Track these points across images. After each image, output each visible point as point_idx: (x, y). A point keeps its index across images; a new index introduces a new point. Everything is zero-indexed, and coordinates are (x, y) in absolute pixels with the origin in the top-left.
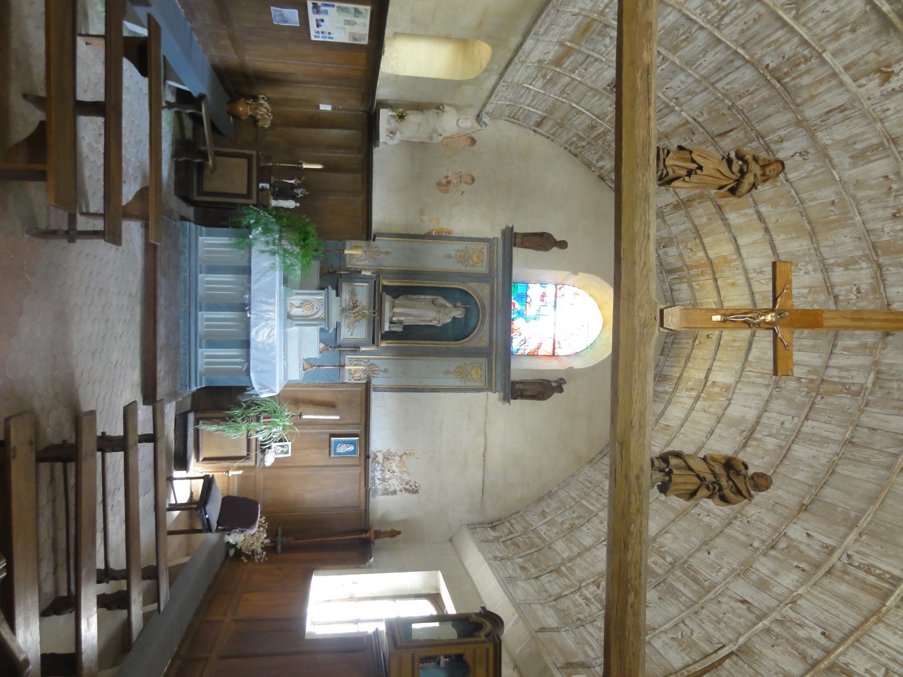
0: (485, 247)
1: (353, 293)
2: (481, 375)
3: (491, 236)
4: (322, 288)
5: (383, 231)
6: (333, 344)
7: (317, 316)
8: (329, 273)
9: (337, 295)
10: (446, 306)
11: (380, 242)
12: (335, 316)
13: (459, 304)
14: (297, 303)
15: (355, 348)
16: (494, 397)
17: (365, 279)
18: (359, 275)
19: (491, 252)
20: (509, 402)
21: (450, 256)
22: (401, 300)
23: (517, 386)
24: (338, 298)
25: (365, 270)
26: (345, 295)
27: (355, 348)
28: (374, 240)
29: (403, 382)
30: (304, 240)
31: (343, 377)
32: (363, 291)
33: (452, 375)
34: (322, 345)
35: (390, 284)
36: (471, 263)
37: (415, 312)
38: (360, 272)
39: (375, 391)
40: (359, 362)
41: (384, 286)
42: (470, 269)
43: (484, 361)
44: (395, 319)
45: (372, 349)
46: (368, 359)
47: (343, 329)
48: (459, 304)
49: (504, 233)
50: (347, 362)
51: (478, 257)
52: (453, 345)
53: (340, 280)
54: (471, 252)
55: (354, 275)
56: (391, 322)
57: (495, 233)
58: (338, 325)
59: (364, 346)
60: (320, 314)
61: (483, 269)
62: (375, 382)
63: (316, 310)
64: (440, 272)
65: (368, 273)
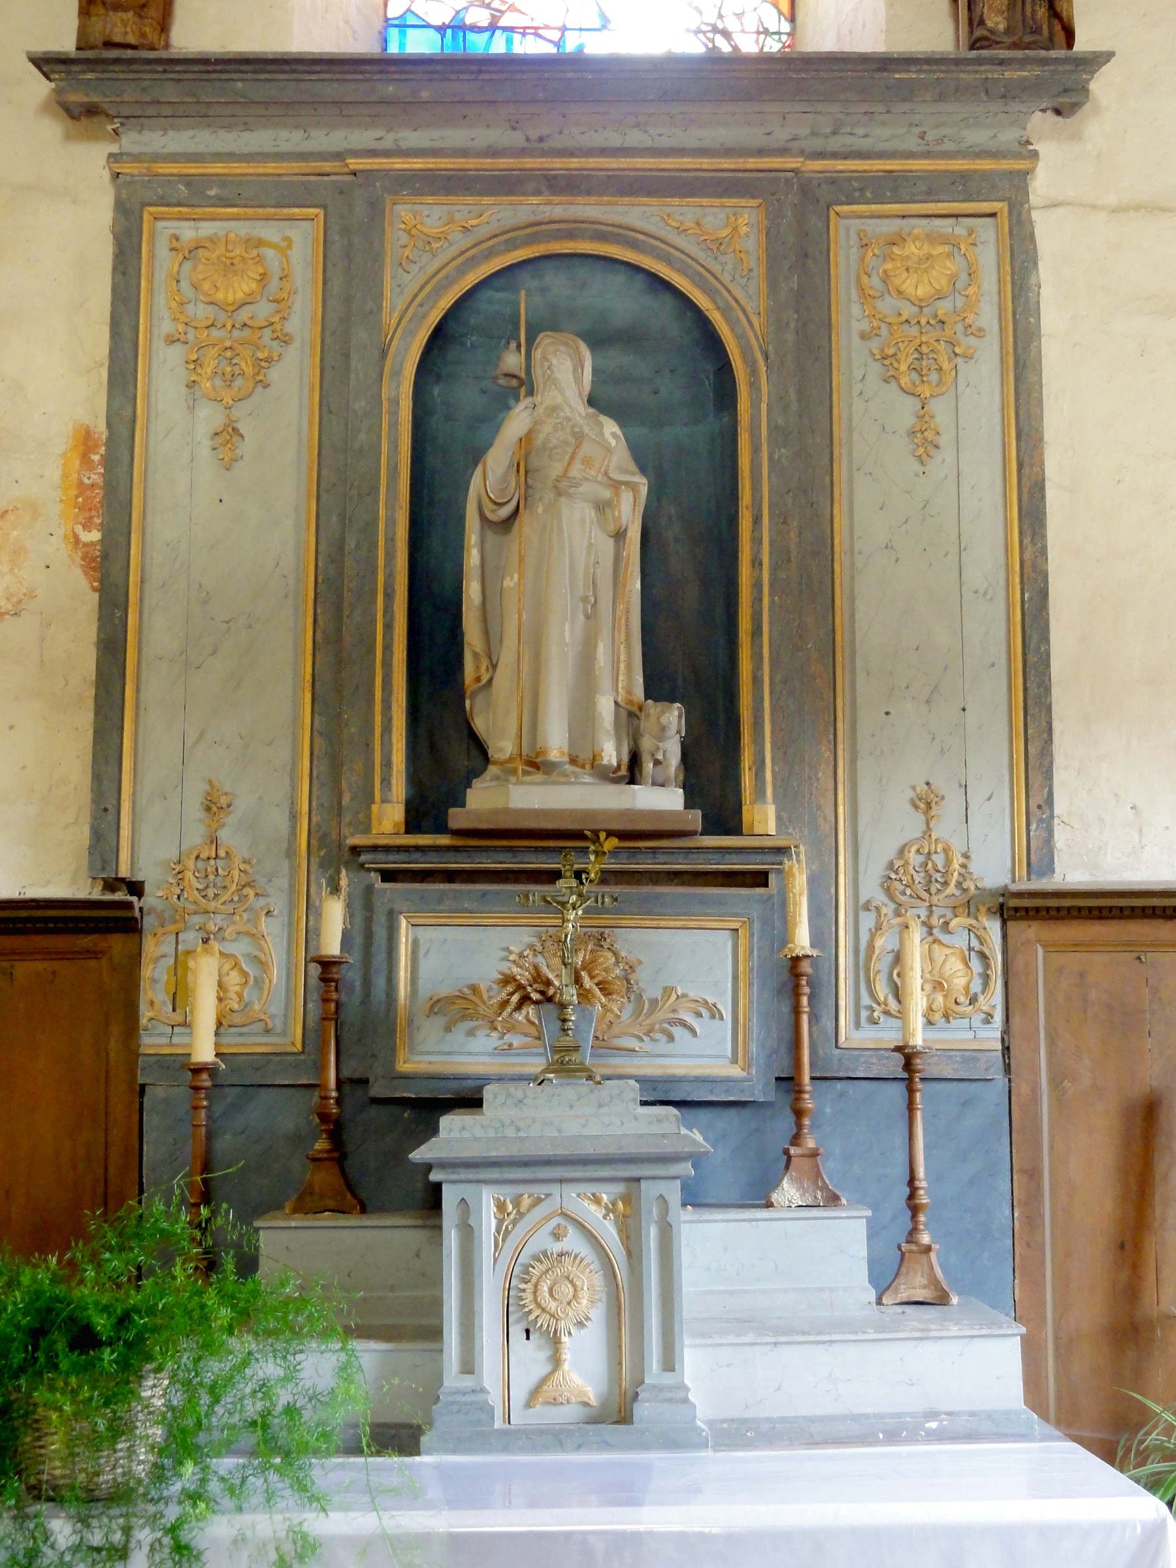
0: (165, 232)
1: (458, 1008)
2: (933, 238)
3: (99, 213)
4: (432, 1199)
5: (84, 835)
6: (771, 1122)
7: (609, 1232)
8: (339, 1153)
9: (471, 1102)
10: (526, 441)
11: (148, 854)
12: (611, 1117)
13: (512, 361)
14: (529, 1359)
15: (794, 984)
16: (1063, 167)
17: (371, 934)
18: (352, 975)
19: (197, 194)
20: (1096, 61)
21: (228, 435)
22: (496, 722)
23: (996, 21)
24: (488, 1093)
25: (312, 934)
26: (471, 1053)
27: (794, 984)
28: (136, 888)
29: (991, 697)
30: (85, 1339)
31: (971, 1056)
32: (450, 951)
33: (940, 410)
34: (788, 1192)
35: (399, 788)
36: (263, 310)
37: (563, 635)
38: (327, 965)
39: (1049, 868)
40: (881, 964)
41: (413, 823)
42: (303, 318)
43: (848, 228)
44: (611, 753)
45: (800, 881)
46: (860, 907)
47: (678, 1066)
48: (512, 361)
49: (82, 115)
50: (887, 1035)
51: (229, 267)
52: (756, 403)
53: (378, 1090)
54: (201, 312)
55: (347, 1001)
56: (632, 772)
57: (83, 172)
58: (661, 1095)
59: (785, 936)
60: (593, 1214)
61: (295, 244)
62: (994, 868)
63: (573, 1242)
64: (321, 489)
65: (334, 917)
